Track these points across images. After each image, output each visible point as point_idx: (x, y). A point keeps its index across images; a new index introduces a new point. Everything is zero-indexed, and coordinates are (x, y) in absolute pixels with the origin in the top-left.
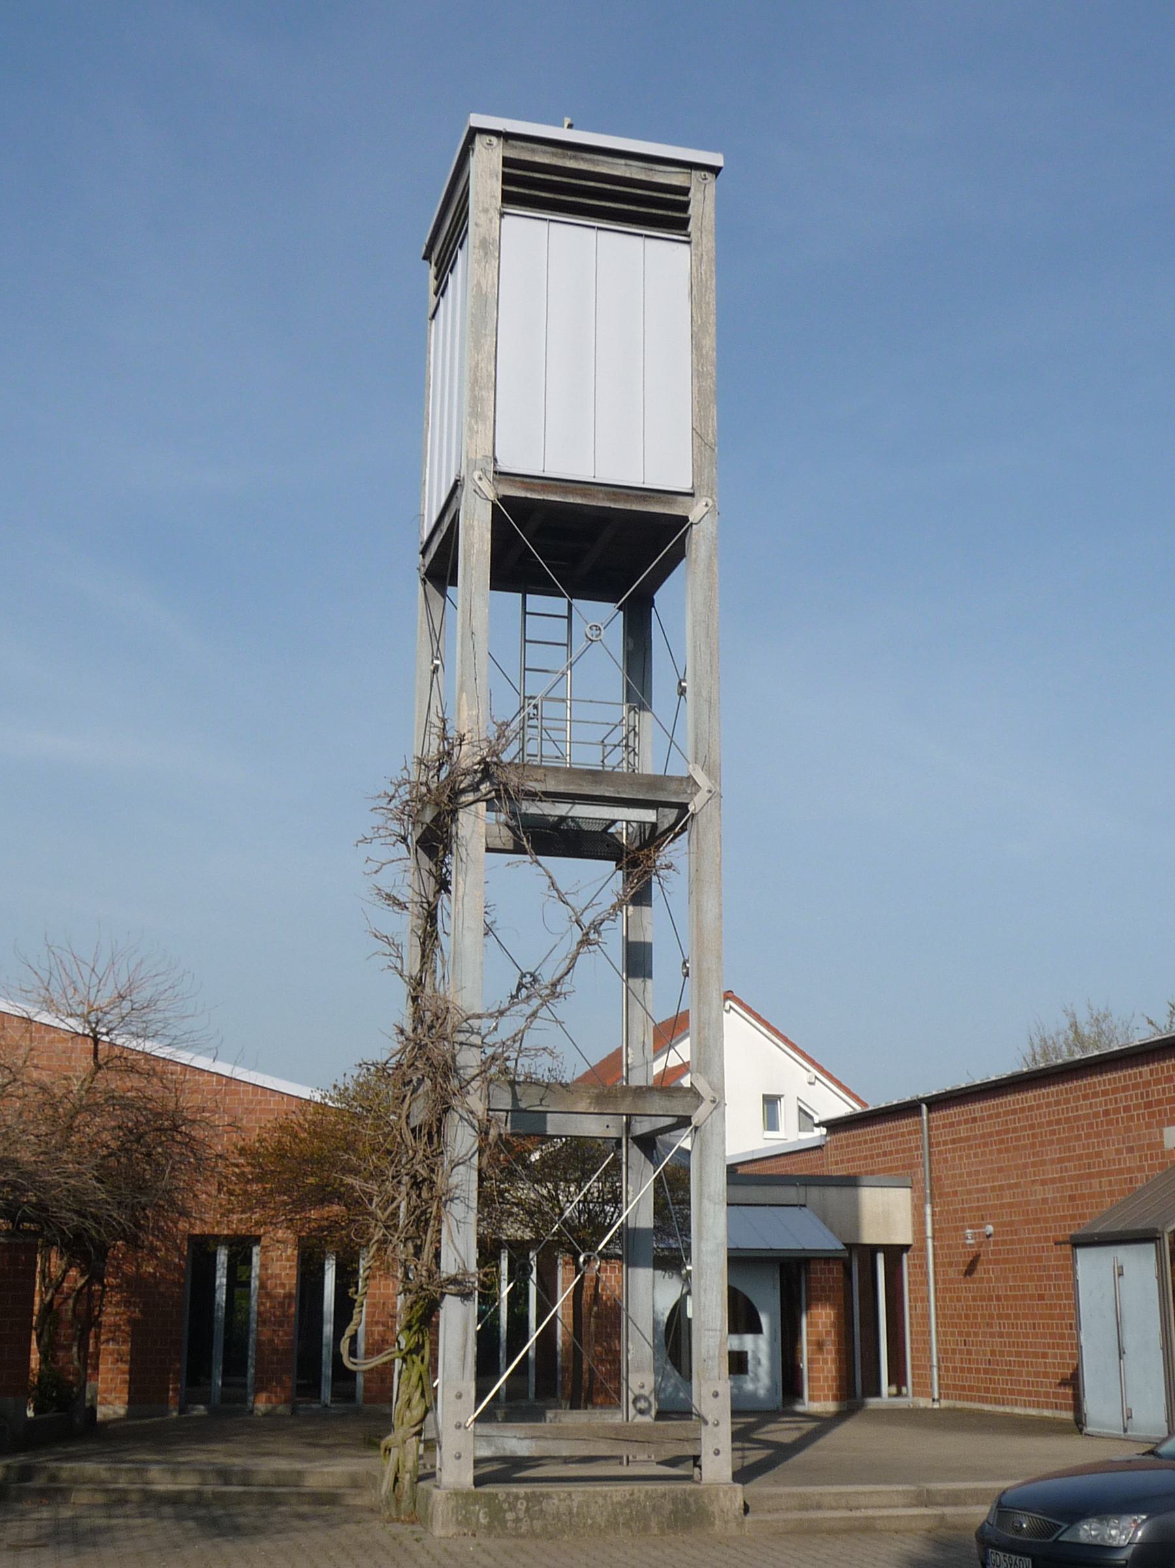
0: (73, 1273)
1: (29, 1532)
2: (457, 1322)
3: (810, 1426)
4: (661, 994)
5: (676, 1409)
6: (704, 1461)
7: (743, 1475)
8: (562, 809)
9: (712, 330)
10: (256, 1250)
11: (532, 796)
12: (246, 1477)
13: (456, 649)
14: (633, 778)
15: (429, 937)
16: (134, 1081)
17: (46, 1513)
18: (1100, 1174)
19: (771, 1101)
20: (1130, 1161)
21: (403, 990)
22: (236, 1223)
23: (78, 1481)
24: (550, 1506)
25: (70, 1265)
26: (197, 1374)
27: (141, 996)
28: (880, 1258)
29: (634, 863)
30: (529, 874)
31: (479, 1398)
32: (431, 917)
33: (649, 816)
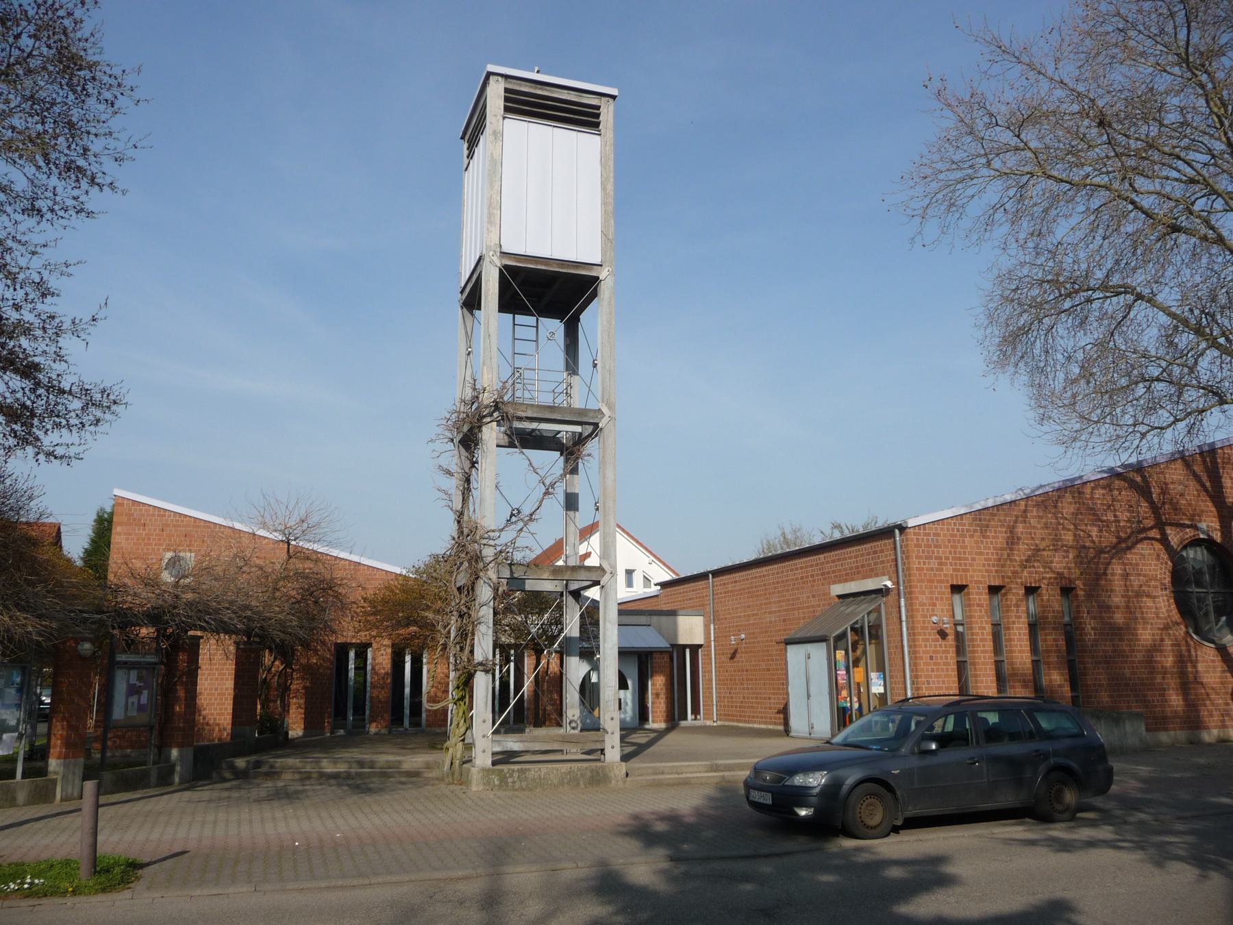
0: (277, 663)
1: (263, 794)
2: (483, 686)
3: (653, 735)
4: (584, 516)
5: (592, 726)
6: (606, 751)
7: (625, 758)
8: (534, 425)
9: (612, 180)
10: (369, 650)
11: (520, 419)
12: (372, 765)
13: (480, 344)
14: (570, 409)
15: (466, 491)
16: (308, 564)
17: (269, 784)
18: (799, 609)
19: (629, 573)
20: (813, 602)
21: (452, 517)
22: (363, 637)
23: (285, 768)
24: (531, 775)
25: (275, 659)
26: (340, 713)
27: (313, 520)
28: (688, 651)
29: (571, 453)
30: (518, 458)
31: (494, 724)
32: (468, 480)
33: (578, 429)
